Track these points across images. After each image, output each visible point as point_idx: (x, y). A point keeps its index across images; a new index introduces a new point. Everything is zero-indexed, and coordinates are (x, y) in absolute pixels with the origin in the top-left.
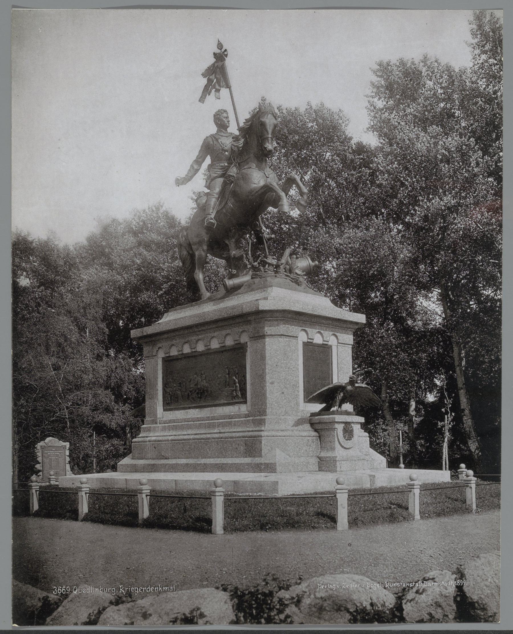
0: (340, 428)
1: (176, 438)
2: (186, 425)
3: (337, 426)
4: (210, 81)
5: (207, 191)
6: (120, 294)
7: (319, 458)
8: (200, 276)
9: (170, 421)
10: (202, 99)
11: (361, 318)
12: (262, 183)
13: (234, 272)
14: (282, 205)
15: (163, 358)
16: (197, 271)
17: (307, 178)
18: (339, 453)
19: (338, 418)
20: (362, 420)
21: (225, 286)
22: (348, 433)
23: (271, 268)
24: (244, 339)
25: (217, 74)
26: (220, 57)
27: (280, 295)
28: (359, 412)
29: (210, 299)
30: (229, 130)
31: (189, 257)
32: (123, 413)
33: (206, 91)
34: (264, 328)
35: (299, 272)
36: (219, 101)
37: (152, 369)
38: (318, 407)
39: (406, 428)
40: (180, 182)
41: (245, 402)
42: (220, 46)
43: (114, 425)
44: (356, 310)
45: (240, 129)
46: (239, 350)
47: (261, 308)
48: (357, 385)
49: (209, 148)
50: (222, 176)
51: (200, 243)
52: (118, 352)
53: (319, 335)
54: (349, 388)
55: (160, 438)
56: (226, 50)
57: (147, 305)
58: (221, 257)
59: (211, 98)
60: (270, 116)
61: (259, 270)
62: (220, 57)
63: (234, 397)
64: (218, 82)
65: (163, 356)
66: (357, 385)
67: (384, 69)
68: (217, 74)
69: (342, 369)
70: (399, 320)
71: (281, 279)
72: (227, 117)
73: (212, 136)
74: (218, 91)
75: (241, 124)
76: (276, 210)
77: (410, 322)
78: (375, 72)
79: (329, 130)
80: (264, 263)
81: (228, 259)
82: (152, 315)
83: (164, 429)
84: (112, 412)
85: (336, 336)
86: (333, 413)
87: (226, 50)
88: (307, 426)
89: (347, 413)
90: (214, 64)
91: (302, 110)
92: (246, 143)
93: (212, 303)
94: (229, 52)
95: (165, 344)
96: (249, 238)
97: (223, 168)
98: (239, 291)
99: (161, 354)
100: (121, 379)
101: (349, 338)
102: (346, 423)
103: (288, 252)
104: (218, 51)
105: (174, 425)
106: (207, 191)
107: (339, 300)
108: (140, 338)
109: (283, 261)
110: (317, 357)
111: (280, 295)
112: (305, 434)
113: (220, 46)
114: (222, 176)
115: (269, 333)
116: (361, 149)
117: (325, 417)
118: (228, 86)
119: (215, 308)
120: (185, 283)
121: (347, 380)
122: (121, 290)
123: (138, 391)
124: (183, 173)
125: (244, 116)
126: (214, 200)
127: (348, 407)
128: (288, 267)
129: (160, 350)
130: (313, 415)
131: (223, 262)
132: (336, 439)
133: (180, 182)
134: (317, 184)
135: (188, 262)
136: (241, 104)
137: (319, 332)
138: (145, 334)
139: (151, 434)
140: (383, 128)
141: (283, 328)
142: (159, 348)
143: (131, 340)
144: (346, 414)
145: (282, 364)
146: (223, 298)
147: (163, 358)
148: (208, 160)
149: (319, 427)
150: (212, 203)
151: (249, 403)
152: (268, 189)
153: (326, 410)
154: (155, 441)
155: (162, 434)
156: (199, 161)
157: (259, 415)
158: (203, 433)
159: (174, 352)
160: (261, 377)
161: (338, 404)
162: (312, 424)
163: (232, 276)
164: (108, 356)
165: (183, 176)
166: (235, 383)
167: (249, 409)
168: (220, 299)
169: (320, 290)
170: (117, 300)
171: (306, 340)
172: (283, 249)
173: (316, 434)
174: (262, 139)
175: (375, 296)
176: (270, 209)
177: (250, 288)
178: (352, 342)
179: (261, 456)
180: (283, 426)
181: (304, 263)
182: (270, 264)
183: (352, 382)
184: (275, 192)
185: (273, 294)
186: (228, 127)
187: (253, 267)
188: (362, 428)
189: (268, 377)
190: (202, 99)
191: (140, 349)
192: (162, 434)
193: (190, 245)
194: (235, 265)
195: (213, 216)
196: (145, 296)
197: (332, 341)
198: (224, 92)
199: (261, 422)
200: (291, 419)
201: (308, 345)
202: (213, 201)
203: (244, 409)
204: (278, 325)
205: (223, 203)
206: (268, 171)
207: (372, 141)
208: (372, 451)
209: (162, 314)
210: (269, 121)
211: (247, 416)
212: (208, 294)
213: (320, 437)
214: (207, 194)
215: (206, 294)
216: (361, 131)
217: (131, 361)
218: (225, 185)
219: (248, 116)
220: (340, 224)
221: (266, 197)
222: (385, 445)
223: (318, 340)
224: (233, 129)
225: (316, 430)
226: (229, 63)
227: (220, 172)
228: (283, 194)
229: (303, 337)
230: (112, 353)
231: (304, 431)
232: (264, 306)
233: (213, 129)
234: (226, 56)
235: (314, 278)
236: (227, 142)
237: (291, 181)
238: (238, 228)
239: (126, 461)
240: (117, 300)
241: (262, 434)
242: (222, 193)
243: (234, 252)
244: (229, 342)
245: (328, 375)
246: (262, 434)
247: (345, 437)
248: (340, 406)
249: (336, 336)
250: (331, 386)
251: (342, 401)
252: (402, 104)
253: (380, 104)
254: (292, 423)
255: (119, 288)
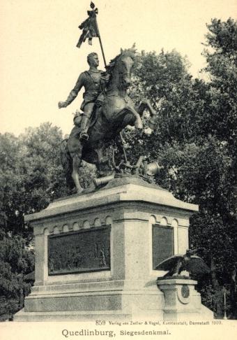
0: (179, 288)
1: (58, 296)
2: (68, 286)
3: (177, 287)
4: (84, 32)
5: (82, 112)
6: (18, 189)
7: (164, 311)
8: (76, 177)
9: (53, 283)
10: (78, 45)
11: (195, 208)
12: (122, 107)
13: (102, 173)
14: (137, 123)
15: (48, 236)
16: (74, 171)
17: (158, 105)
18: (179, 307)
19: (178, 281)
20: (195, 282)
21: (95, 183)
22: (186, 293)
23: (129, 170)
24: (109, 221)
25: (89, 28)
26: (92, 14)
27: (134, 190)
28: (192, 277)
29: (83, 193)
30: (99, 68)
31: (68, 162)
32: (18, 279)
33: (82, 40)
34: (123, 213)
35: (150, 174)
36: (92, 47)
37: (40, 245)
38: (162, 273)
39: (229, 292)
40: (62, 106)
41: (109, 269)
42: (92, 5)
43: (11, 288)
44: (193, 202)
45: (106, 67)
46: (105, 230)
47: (122, 199)
48: (192, 257)
49: (83, 82)
50: (93, 101)
51: (76, 152)
52: (14, 234)
53: (164, 220)
54: (186, 259)
55: (46, 296)
56: (97, 9)
57: (37, 198)
58: (92, 163)
59: (85, 44)
60: (129, 58)
61: (120, 172)
62: (92, 14)
63: (100, 266)
64: (91, 31)
65: (49, 234)
66: (192, 257)
67: (216, 25)
68: (89, 28)
69: (181, 244)
70: (224, 212)
71: (134, 179)
72: (97, 59)
73: (86, 72)
74: (90, 39)
75: (108, 64)
76: (133, 128)
77: (232, 213)
78: (209, 27)
79: (173, 68)
80: (123, 167)
81: (97, 165)
82: (39, 205)
83: (49, 289)
84: (10, 279)
85: (177, 221)
86: (175, 278)
87: (97, 9)
88: (156, 286)
89: (185, 278)
90: (87, 20)
91: (157, 54)
92: (111, 78)
93: (85, 196)
94: (99, 11)
95: (50, 226)
96: (113, 150)
97: (94, 95)
98: (106, 187)
99: (47, 233)
100: (17, 254)
101: (185, 222)
102: (184, 285)
103: (141, 158)
104: (91, 9)
105: (57, 286)
106: (82, 112)
107: (180, 196)
108: (31, 221)
109: (138, 165)
110: (163, 236)
111: (134, 190)
112: (153, 293)
113: (92, 5)
114: (93, 101)
115: (127, 217)
116: (198, 83)
117: (169, 281)
118: (98, 36)
119: (88, 199)
120: (65, 182)
121: (185, 253)
122: (19, 186)
123: (29, 264)
124: (64, 99)
125: (111, 55)
126: (87, 119)
127: (185, 273)
128: (141, 170)
129: (46, 230)
130: (159, 279)
131: (93, 166)
132: (176, 297)
133: (62, 106)
134: (167, 110)
135: (67, 166)
136: (109, 47)
137: (165, 218)
138: (35, 218)
139: (38, 293)
140: (214, 66)
141: (137, 214)
142: (45, 229)
143: (25, 225)
144: (184, 278)
145: (135, 240)
146: (93, 192)
147: (48, 236)
148: (83, 90)
149: (163, 286)
150: (86, 122)
151: (112, 269)
152: (127, 111)
153: (169, 275)
154: (42, 298)
155: (47, 293)
156: (76, 90)
157: (120, 278)
158: (77, 291)
159: (56, 232)
160: (121, 253)
161: (178, 271)
162: (158, 286)
163: (100, 176)
164: (7, 236)
165: (64, 101)
166: (102, 255)
167: (112, 274)
168: (91, 192)
169: (165, 188)
170: (15, 194)
171: (154, 223)
172: (138, 158)
173: (162, 293)
174: (122, 75)
175: (208, 194)
176: (129, 127)
177: (114, 185)
178: (188, 224)
179: (120, 309)
180: (137, 287)
181: (153, 167)
182: (128, 168)
183: (188, 254)
184: (132, 113)
185: (130, 189)
186: (98, 66)
187: (116, 170)
188: (195, 289)
189: (126, 251)
190: (78, 45)
191: (31, 230)
192: (47, 293)
193: (68, 153)
194: (102, 168)
195: (86, 131)
196: (36, 192)
197: (174, 224)
198: (95, 40)
199: (122, 284)
200: (143, 282)
201: (156, 227)
202: (86, 120)
203: (107, 274)
204: (134, 211)
205: (93, 123)
206: (127, 98)
207: (207, 78)
208: (203, 306)
209: (48, 204)
210: (128, 62)
211: (111, 279)
212: (82, 189)
213: (164, 295)
214: (82, 115)
215: (81, 190)
216: (197, 68)
217: (25, 240)
218: (95, 108)
219: (113, 58)
220: (180, 141)
221: (123, 119)
222: (213, 304)
223: (163, 223)
224: (102, 67)
225: (161, 290)
226: (99, 19)
227: (92, 98)
228: (138, 115)
229: (152, 221)
230: (10, 234)
231: (152, 290)
232: (124, 197)
233: (87, 68)
234: (97, 13)
235: (160, 179)
236: (97, 77)
237: (144, 107)
238: (102, 137)
239: (21, 313)
240: (15, 194)
241: (122, 292)
242: (93, 116)
243: (101, 159)
244: (98, 224)
245: (171, 248)
246: (122, 292)
247: (183, 295)
248: (179, 273)
249: (177, 221)
250: (173, 257)
251: (181, 270)
252: (228, 52)
253: (212, 50)
254: (144, 285)
255: (17, 185)
